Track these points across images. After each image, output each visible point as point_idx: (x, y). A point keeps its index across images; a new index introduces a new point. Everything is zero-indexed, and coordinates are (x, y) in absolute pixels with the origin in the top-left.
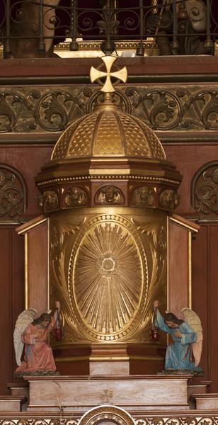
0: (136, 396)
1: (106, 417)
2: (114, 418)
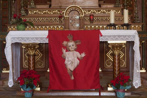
0: (83, 3)
1: (74, 9)
2: (76, 9)
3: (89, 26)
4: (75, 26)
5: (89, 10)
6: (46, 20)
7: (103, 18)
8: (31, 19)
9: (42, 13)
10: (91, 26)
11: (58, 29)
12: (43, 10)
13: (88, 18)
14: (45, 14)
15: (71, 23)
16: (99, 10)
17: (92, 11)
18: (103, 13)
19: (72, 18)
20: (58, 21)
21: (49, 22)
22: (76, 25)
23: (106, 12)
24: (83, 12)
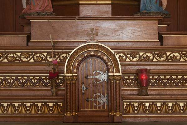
0: (117, 33)
3: (136, 102)
4: (95, 102)
5: (132, 52)
6: (13, 83)
7: (173, 77)
8: (19, 78)
9: (32, 60)
10: (142, 102)
11: (22, 110)
12: (6, 52)
13: (133, 77)
14: (14, 62)
15: (83, 94)
16: (160, 52)
17: (141, 54)
18: (171, 59)
19: (88, 79)
20: (46, 86)
21: (23, 86)
22: (98, 100)
23: (181, 57)
24: (117, 57)
